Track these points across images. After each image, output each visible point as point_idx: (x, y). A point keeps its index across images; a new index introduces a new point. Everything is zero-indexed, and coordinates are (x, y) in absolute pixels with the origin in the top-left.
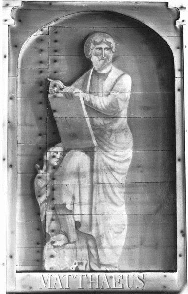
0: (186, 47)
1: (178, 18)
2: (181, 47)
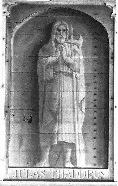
0: (116, 33)
1: (112, 12)
2: (113, 30)
